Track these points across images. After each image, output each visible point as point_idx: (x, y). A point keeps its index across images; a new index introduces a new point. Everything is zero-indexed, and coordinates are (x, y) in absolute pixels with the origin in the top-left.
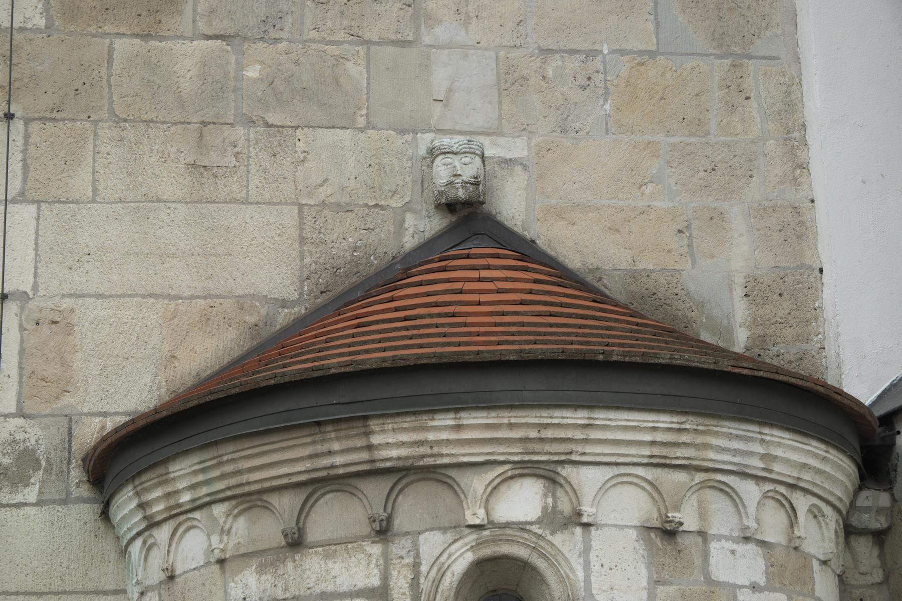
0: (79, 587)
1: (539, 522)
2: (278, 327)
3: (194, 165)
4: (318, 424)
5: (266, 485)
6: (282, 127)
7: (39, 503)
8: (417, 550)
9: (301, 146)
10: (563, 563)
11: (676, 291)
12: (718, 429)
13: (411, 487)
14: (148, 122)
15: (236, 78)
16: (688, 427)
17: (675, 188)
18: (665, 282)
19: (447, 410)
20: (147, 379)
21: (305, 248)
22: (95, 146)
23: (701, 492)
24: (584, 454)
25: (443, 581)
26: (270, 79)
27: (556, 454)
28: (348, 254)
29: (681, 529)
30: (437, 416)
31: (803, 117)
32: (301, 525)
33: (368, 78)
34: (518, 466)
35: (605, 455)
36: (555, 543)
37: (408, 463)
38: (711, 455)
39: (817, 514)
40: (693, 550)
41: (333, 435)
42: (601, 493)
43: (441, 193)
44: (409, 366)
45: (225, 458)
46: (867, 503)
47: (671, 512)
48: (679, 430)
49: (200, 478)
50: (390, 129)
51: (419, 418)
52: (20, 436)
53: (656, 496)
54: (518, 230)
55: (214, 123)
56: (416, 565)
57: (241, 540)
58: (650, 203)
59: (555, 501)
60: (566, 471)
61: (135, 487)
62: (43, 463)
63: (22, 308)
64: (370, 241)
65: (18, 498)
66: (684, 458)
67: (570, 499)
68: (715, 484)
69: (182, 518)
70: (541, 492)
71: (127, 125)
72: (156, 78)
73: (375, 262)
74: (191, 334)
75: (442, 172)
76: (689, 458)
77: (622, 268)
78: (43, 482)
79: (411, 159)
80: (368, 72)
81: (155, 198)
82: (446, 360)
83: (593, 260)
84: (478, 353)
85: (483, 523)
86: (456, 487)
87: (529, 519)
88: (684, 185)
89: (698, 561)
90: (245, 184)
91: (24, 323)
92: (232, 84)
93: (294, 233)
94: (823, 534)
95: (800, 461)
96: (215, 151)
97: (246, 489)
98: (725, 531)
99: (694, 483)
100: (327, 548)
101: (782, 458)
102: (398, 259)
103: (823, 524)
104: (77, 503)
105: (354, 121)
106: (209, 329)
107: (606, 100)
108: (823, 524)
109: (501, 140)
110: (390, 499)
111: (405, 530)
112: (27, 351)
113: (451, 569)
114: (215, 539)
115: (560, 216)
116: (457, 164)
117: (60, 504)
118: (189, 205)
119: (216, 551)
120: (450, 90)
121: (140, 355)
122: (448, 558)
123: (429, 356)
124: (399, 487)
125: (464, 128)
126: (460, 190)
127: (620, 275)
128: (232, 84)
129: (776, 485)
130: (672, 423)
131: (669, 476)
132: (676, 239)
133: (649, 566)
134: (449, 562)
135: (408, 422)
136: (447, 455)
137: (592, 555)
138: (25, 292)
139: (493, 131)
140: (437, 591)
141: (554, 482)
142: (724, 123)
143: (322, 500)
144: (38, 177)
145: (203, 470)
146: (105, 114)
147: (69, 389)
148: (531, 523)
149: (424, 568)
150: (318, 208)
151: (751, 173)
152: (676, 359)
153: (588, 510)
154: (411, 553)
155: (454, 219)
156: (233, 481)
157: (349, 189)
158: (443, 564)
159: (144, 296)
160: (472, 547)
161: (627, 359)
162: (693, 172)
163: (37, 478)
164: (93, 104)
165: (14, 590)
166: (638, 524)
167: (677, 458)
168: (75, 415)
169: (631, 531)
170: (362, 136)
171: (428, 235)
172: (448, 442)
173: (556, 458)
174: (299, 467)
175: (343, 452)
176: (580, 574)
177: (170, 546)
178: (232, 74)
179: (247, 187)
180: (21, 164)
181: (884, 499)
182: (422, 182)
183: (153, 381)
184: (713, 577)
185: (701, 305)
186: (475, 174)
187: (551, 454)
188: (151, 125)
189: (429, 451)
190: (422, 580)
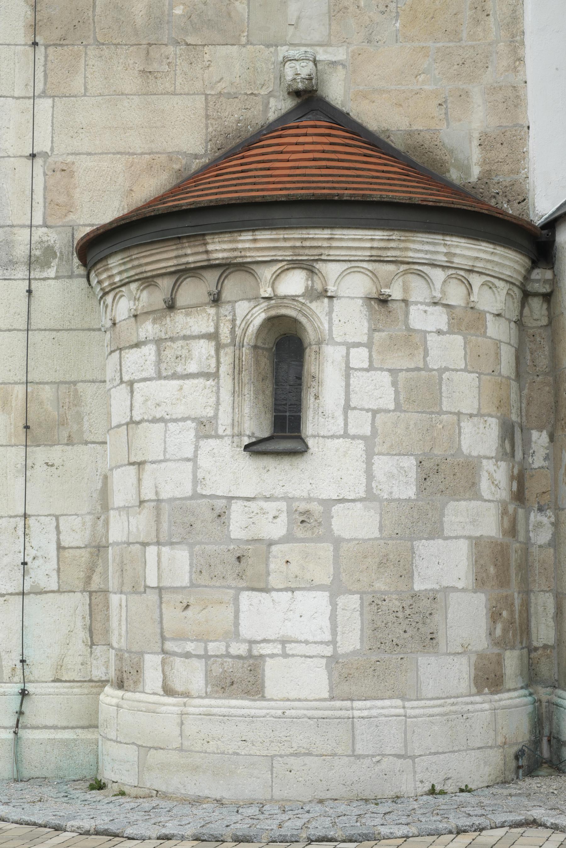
0: (79, 327)
1: (303, 295)
2: (193, 171)
3: (143, 71)
4: (179, 238)
5: (154, 273)
6: (196, 45)
7: (56, 278)
8: (235, 311)
9: (207, 57)
10: (316, 319)
11: (436, 143)
12: (415, 238)
13: (232, 275)
14: (116, 45)
15: (169, 15)
16: (394, 238)
17: (438, 77)
18: (429, 137)
19: (248, 231)
20: (116, 204)
21: (209, 122)
22: (86, 61)
23: (405, 276)
24: (329, 255)
25: (248, 330)
26: (189, 15)
27: (312, 255)
28: (234, 125)
29: (390, 299)
30: (243, 234)
31: (523, 26)
32: (173, 296)
33: (249, 12)
34: (291, 263)
35: (342, 256)
36: (312, 308)
37: (228, 261)
38: (411, 254)
39: (491, 286)
40: (399, 311)
41: (187, 245)
42: (340, 278)
43: (289, 85)
44: (225, 205)
45: (133, 257)
46: (538, 277)
47: (384, 288)
48: (388, 240)
49: (123, 268)
50: (261, 44)
51: (233, 235)
52: (45, 238)
53: (375, 279)
54: (339, 106)
55: (155, 44)
56: (234, 320)
57: (145, 304)
58: (422, 87)
59: (313, 283)
60: (319, 265)
61: (95, 272)
62: (58, 254)
63: (45, 162)
64: (248, 116)
65: (45, 275)
66: (392, 256)
67: (322, 282)
68: (415, 271)
69: (117, 290)
70: (305, 278)
71: (104, 47)
72: (121, 17)
73: (251, 129)
74: (141, 177)
75: (289, 72)
76: (395, 257)
77: (402, 129)
78: (58, 266)
79: (273, 63)
80: (249, 8)
81: (120, 93)
82: (245, 201)
83: (385, 125)
84: (263, 197)
85: (270, 296)
86: (256, 275)
87: (297, 294)
88: (444, 74)
89: (401, 317)
90: (173, 82)
91: (46, 171)
92: (166, 18)
93: (203, 112)
94: (496, 298)
95: (473, 255)
96: (156, 62)
97: (145, 275)
98: (420, 299)
99: (399, 271)
100: (187, 310)
101: (460, 254)
102: (265, 127)
103: (496, 292)
104: (77, 278)
105: (239, 40)
106: (152, 173)
107: (397, 20)
108: (496, 292)
109: (330, 49)
110: (220, 282)
111: (228, 300)
112: (48, 188)
113: (253, 323)
114: (132, 303)
115: (365, 97)
116: (298, 67)
117: (68, 278)
118: (140, 97)
119: (132, 310)
120: (299, 18)
121: (112, 190)
122: (251, 317)
123: (236, 199)
124: (225, 275)
125: (308, 42)
126: (300, 83)
127: (401, 134)
128: (166, 18)
129: (457, 271)
130: (384, 236)
131: (383, 268)
132: (437, 109)
133: (369, 321)
134: (252, 318)
135: (226, 237)
136: (250, 257)
137: (334, 315)
138: (46, 152)
139: (325, 43)
140: (245, 335)
141: (312, 272)
142: (471, 33)
143: (185, 282)
144: (53, 81)
145: (124, 264)
146: (91, 41)
147: (72, 210)
148: (299, 296)
149: (238, 322)
150: (216, 96)
151: (487, 65)
152: (384, 198)
153: (332, 289)
154: (231, 313)
155: (299, 101)
156: (138, 270)
157: (235, 84)
158: (249, 320)
159: (114, 154)
160: (265, 310)
161: (353, 199)
162: (450, 65)
163: (55, 263)
164: (84, 34)
165: (43, 328)
166: (364, 296)
167: (388, 257)
168: (76, 226)
169: (359, 300)
170: (244, 50)
171: (283, 111)
172: (250, 249)
173: (312, 258)
174: (171, 263)
175: (193, 254)
176: (326, 326)
177: (112, 306)
178: (166, 12)
179: (175, 84)
180: (43, 74)
181: (548, 275)
182: (280, 78)
183: (120, 205)
184: (411, 327)
185: (452, 151)
186: (309, 73)
187: (309, 255)
188: (118, 46)
189: (239, 254)
190: (237, 329)
